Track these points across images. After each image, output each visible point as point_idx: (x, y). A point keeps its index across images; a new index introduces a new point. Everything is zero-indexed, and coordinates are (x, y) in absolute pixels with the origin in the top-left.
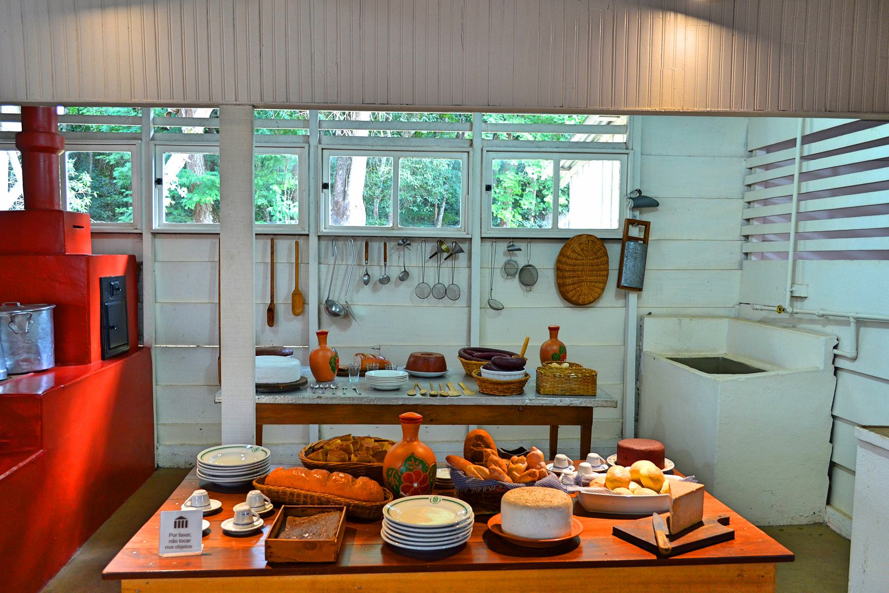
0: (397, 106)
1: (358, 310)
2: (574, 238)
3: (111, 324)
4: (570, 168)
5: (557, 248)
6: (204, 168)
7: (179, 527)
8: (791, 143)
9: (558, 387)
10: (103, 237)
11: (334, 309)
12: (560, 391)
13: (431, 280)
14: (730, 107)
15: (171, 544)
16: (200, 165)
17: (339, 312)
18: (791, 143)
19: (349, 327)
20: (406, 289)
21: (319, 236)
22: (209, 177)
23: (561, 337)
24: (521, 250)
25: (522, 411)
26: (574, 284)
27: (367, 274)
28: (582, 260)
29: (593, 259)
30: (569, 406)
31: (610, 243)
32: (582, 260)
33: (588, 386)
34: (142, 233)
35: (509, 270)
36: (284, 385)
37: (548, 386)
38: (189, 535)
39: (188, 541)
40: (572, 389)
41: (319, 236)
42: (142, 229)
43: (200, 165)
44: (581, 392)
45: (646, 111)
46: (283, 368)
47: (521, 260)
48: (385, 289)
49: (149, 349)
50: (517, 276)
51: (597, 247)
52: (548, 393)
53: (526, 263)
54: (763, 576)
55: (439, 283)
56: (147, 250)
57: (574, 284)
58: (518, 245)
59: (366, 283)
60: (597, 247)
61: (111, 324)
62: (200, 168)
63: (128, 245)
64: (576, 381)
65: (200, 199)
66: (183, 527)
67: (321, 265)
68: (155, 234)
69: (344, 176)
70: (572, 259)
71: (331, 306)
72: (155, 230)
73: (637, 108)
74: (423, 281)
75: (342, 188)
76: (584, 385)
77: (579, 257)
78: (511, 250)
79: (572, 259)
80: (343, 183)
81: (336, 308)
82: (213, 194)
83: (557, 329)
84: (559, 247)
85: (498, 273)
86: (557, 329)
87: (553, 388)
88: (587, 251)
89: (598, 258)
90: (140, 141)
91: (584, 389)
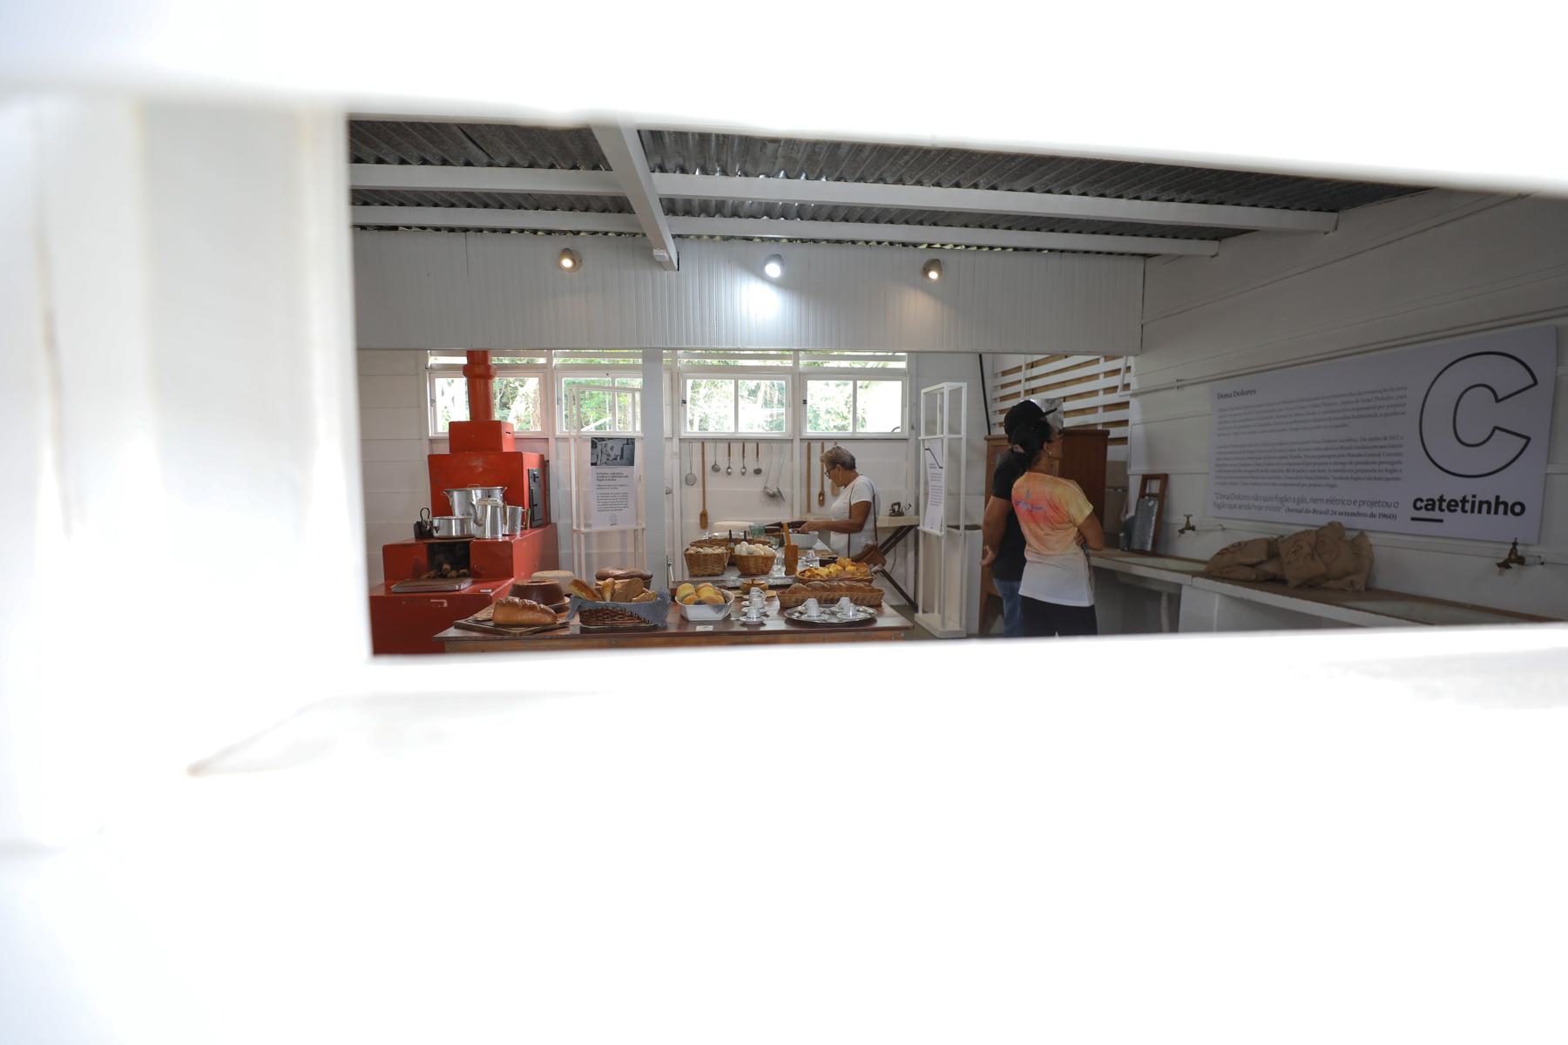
3: (535, 503)
4: (867, 387)
7: (1217, 465)
8: (1019, 369)
18: (1019, 369)
21: (680, 439)
41: (680, 439)
49: (555, 524)
61: (535, 503)
63: (540, 447)
66: (1217, 465)
68: (557, 439)
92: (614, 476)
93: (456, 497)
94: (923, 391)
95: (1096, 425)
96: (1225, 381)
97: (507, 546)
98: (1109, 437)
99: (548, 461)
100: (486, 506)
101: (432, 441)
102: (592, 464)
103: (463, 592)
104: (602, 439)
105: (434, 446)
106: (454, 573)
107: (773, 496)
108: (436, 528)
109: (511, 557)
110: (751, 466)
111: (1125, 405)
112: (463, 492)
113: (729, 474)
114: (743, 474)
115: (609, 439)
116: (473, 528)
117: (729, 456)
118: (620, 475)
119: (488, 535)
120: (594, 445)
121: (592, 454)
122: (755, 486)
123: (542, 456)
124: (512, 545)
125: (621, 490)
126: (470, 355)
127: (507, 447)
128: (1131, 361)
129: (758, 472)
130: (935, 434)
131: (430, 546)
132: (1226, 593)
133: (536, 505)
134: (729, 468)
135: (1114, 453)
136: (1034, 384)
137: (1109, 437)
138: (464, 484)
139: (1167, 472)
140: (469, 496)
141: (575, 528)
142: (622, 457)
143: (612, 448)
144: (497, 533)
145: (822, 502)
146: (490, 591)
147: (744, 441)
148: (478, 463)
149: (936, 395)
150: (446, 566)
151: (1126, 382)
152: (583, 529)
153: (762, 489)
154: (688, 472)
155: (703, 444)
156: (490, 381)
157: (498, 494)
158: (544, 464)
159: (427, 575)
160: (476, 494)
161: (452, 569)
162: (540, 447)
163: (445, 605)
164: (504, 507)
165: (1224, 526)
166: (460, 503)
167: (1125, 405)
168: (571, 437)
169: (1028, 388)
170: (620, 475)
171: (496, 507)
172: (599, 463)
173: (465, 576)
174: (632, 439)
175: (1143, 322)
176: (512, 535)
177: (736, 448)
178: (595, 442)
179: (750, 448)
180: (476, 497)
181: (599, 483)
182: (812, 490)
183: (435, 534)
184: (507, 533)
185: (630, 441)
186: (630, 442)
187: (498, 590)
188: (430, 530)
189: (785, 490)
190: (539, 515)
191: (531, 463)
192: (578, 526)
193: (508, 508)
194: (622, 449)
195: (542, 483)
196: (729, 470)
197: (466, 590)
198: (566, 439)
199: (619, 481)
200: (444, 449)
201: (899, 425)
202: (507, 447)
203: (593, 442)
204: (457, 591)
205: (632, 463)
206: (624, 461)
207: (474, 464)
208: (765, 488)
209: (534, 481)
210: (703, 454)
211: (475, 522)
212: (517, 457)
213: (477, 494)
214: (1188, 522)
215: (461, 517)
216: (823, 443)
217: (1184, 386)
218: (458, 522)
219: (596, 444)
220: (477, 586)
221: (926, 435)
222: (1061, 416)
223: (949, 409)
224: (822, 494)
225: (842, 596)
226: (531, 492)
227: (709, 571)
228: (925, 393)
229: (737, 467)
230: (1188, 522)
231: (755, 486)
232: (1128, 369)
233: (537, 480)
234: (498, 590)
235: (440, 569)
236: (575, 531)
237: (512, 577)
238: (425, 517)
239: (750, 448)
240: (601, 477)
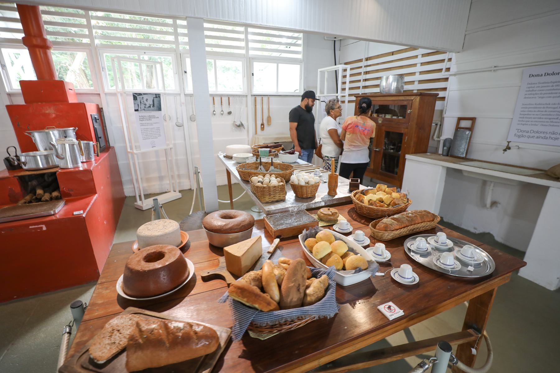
3: (99, 136)
63: (95, 99)
68: (106, 94)
92: (150, 118)
93: (37, 137)
94: (319, 70)
95: (413, 90)
96: (537, 66)
97: (87, 172)
98: (439, 96)
99: (102, 108)
100: (64, 144)
101: (9, 95)
102: (136, 110)
103: (58, 216)
104: (140, 94)
105: (13, 98)
106: (47, 196)
107: (239, 126)
108: (23, 163)
109: (93, 180)
110: (226, 111)
111: (446, 79)
112: (41, 133)
113: (215, 114)
114: (222, 114)
115: (144, 94)
116: (57, 161)
117: (214, 104)
118: (154, 117)
119: (70, 165)
120: (135, 98)
121: (135, 104)
122: (229, 121)
123: (98, 105)
124: (91, 171)
125: (155, 126)
126: (21, 9)
127: (72, 100)
128: (453, 56)
129: (230, 113)
130: (324, 94)
131: (21, 178)
132: (443, 165)
133: (100, 138)
134: (214, 111)
135: (438, 105)
136: (369, 69)
137: (439, 96)
138: (41, 127)
139: (476, 117)
140: (48, 136)
141: (129, 150)
142: (153, 106)
143: (147, 100)
144: (77, 163)
145: (263, 129)
146: (82, 212)
147: (221, 96)
148: (51, 111)
149: (325, 72)
150: (39, 191)
151: (447, 67)
152: (135, 151)
153: (233, 123)
154: (191, 113)
156: (48, 51)
157: (71, 131)
158: (100, 110)
159: (23, 201)
160: (53, 134)
161: (45, 192)
162: (95, 99)
163: (44, 228)
164: (79, 144)
165: (520, 147)
166: (41, 140)
167: (446, 79)
168: (119, 92)
169: (365, 71)
170: (154, 117)
171: (73, 145)
172: (139, 109)
173: (58, 199)
174: (158, 94)
175: (467, 33)
176: (88, 162)
177: (217, 100)
178: (136, 96)
179: (225, 100)
180: (54, 136)
181: (141, 122)
182: (257, 122)
183: (24, 167)
184: (84, 161)
185: (157, 96)
186: (158, 96)
187: (88, 209)
188: (19, 164)
189: (244, 123)
190: (103, 144)
191: (91, 111)
192: (131, 148)
193: (82, 142)
194: (153, 101)
195: (101, 123)
196: (214, 113)
197: (61, 213)
198: (114, 94)
199: (153, 120)
200: (20, 101)
201: (298, 88)
202: (72, 100)
203: (134, 96)
204: (53, 215)
205: (160, 109)
206: (155, 108)
207: (47, 112)
208: (234, 122)
209: (96, 122)
211: (58, 156)
212: (82, 106)
213: (54, 134)
214: (508, 145)
215: (45, 153)
216: (262, 98)
217: (497, 70)
218: (43, 157)
219: (136, 97)
220: (71, 206)
221: (320, 94)
222: (403, 84)
223: (321, 81)
224: (262, 124)
225: (441, 230)
226: (95, 130)
227: (277, 198)
228: (320, 71)
229: (218, 111)
230: (508, 145)
231: (229, 121)
232: (450, 60)
233: (98, 121)
234: (88, 209)
235: (35, 193)
236: (129, 152)
237: (96, 193)
238: (13, 155)
239: (225, 100)
240: (142, 118)
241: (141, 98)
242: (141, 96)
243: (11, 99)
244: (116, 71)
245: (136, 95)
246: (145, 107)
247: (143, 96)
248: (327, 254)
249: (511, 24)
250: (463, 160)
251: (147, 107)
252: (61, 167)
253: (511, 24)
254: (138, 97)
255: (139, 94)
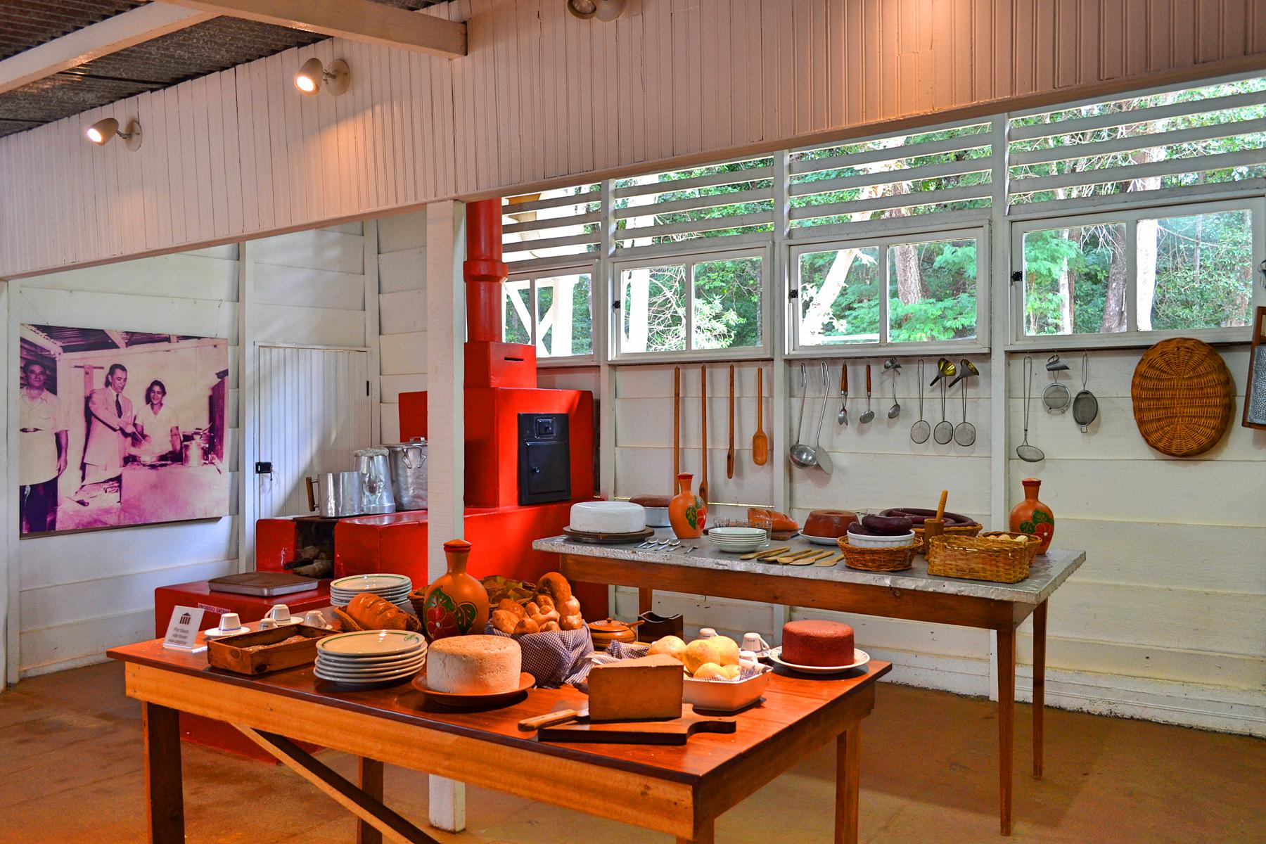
0: (577, 174)
1: (841, 459)
2: (1157, 345)
5: (1131, 363)
6: (920, 295)
9: (951, 565)
10: (573, 372)
11: (804, 457)
12: (954, 570)
13: (933, 416)
14: (1012, 92)
15: (173, 638)
16: (915, 291)
17: (810, 461)
19: (828, 483)
20: (901, 430)
22: (924, 307)
23: (1044, 497)
24: (1068, 368)
25: (899, 597)
26: (1159, 420)
27: (844, 409)
28: (1170, 379)
29: (1191, 378)
30: (956, 595)
31: (1238, 351)
32: (1170, 379)
33: (997, 567)
34: (599, 366)
35: (1054, 403)
36: (605, 535)
37: (937, 561)
38: (187, 632)
39: (185, 637)
40: (972, 570)
42: (599, 361)
43: (915, 291)
44: (988, 575)
45: (876, 125)
46: (607, 514)
47: (1074, 386)
48: (873, 429)
50: (1071, 409)
51: (1196, 359)
52: (938, 573)
53: (1081, 389)
54: (676, 803)
55: (944, 421)
56: (603, 387)
57: (1159, 420)
58: (1063, 361)
59: (843, 421)
60: (1196, 359)
62: (916, 296)
64: (977, 558)
65: (909, 337)
67: (793, 399)
69: (1121, 290)
70: (1151, 379)
71: (801, 452)
72: (612, 360)
73: (864, 122)
74: (964, 420)
75: (1117, 309)
76: (991, 565)
77: (1165, 376)
78: (1055, 369)
79: (1151, 379)
80: (1118, 300)
81: (807, 455)
82: (927, 329)
83: (1037, 484)
84: (1131, 363)
85: (1038, 406)
86: (1037, 484)
87: (945, 566)
88: (1178, 365)
89: (1199, 376)
90: (597, 260)
91: (991, 571)
115: (134, 339)
155: (677, 371)
156: (495, 284)
210: (238, 449)
241: (99, 378)
242: (104, 358)
243: (790, 403)
244: (578, 354)
245: (53, 347)
246: (129, 460)
247: (124, 355)
248: (599, 464)
249: (197, 179)
250: (307, 578)
251: (148, 459)
252: (433, 823)
253: (197, 179)
254: (68, 366)
255: (83, 332)
